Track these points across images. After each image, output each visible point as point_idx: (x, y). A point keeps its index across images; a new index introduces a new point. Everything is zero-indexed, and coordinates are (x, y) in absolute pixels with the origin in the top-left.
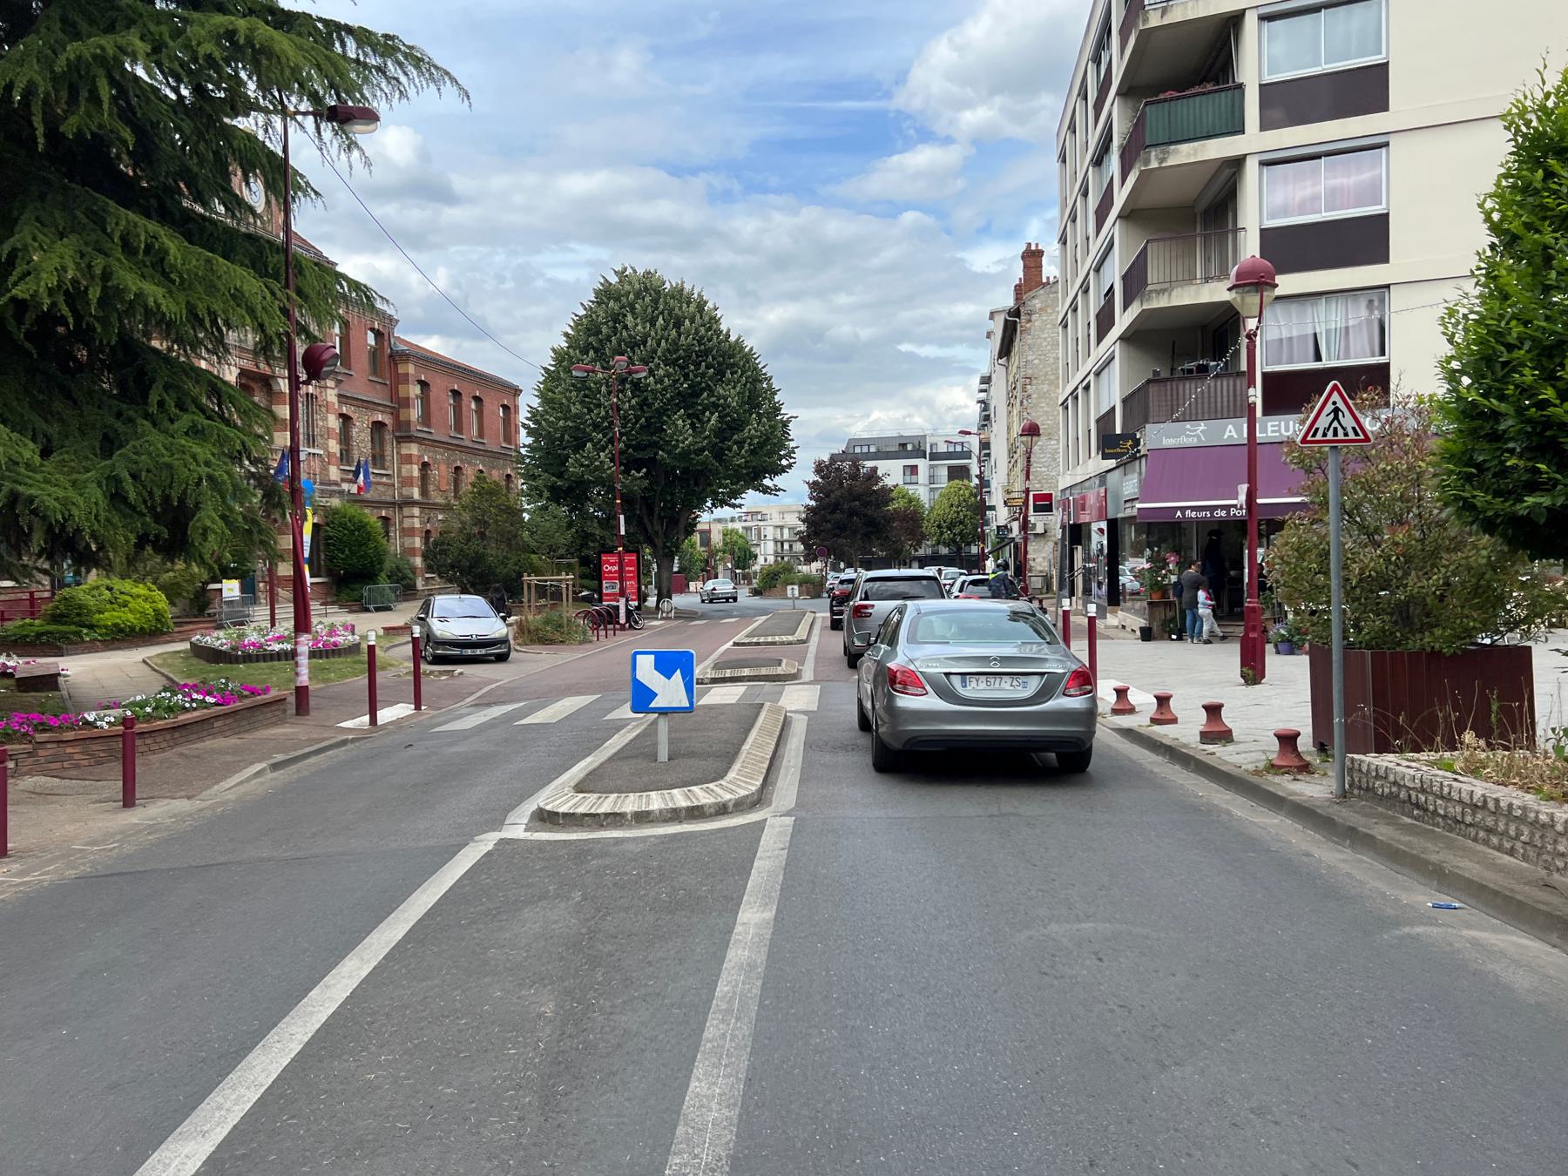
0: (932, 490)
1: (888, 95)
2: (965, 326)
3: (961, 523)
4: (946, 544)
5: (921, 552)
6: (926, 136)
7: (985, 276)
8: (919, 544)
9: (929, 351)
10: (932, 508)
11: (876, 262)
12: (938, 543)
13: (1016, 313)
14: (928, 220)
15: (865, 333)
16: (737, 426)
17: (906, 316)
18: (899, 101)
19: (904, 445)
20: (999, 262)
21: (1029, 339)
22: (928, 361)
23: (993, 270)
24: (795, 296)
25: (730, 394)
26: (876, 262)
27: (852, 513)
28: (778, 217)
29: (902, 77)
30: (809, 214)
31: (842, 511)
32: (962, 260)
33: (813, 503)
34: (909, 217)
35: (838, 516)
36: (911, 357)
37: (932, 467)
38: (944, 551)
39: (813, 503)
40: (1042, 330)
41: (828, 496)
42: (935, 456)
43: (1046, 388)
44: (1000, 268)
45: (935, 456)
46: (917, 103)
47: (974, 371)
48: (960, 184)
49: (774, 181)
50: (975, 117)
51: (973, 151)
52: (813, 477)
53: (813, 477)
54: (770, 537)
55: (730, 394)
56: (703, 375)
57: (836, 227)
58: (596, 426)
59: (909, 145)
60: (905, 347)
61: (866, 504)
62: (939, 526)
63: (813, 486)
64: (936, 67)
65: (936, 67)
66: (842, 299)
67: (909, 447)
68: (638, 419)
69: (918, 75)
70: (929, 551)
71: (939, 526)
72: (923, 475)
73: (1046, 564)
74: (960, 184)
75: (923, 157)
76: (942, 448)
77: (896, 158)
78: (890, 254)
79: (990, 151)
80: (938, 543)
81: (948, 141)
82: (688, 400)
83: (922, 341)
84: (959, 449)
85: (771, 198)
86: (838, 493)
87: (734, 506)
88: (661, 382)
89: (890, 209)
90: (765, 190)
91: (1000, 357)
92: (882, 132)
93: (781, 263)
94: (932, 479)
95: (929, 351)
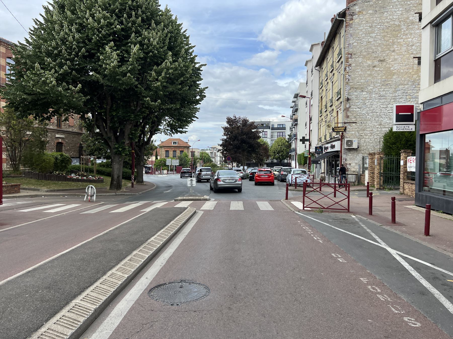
0: (272, 140)
1: (257, 37)
2: (277, 101)
3: (282, 152)
4: (277, 159)
5: (268, 162)
6: (266, 48)
7: (283, 87)
8: (268, 158)
9: (267, 107)
10: (272, 146)
11: (253, 82)
12: (274, 158)
13: (343, 14)
14: (267, 71)
15: (249, 102)
16: (158, 60)
17: (261, 97)
18: (259, 39)
19: (263, 124)
20: (286, 83)
21: (351, 30)
22: (266, 110)
23: (285, 86)
24: (230, 91)
25: (154, 36)
26: (253, 82)
27: (243, 141)
28: (227, 69)
29: (260, 32)
30: (235, 68)
31: (238, 140)
32: (277, 83)
33: (225, 137)
34: (262, 70)
35: (236, 142)
36: (262, 109)
37: (272, 132)
38: (275, 161)
39: (225, 137)
40: (359, 25)
41: (232, 133)
42: (273, 129)
43: (360, 60)
44: (287, 85)
45: (273, 129)
46: (265, 39)
47: (279, 113)
48: (277, 62)
49: (225, 59)
50: (281, 43)
51: (280, 53)
52: (227, 125)
53: (227, 125)
54: (218, 155)
55: (154, 36)
56: (134, 23)
57: (242, 72)
58: (49, 54)
59: (262, 50)
60: (260, 106)
61: (250, 138)
62: (274, 153)
63: (225, 129)
64: (270, 28)
65: (270, 28)
66: (243, 92)
67: (265, 125)
68: (80, 48)
69: (265, 31)
70: (270, 161)
71: (274, 153)
72: (269, 135)
73: (357, 167)
74: (277, 62)
75: (267, 54)
76: (276, 126)
77: (259, 54)
78: (257, 80)
79: (285, 53)
80: (274, 158)
81: (273, 50)
82: (121, 40)
83: (265, 105)
84: (281, 126)
85: (225, 63)
86: (236, 131)
87: (181, 132)
88: (99, 22)
89: (258, 68)
90: (223, 61)
91: (316, 66)
92: (257, 47)
93: (227, 81)
94: (272, 136)
95: (267, 107)
